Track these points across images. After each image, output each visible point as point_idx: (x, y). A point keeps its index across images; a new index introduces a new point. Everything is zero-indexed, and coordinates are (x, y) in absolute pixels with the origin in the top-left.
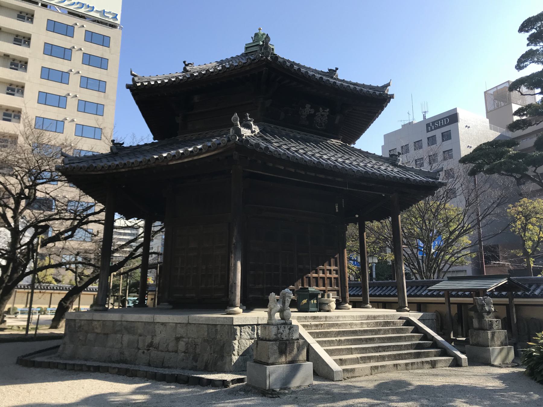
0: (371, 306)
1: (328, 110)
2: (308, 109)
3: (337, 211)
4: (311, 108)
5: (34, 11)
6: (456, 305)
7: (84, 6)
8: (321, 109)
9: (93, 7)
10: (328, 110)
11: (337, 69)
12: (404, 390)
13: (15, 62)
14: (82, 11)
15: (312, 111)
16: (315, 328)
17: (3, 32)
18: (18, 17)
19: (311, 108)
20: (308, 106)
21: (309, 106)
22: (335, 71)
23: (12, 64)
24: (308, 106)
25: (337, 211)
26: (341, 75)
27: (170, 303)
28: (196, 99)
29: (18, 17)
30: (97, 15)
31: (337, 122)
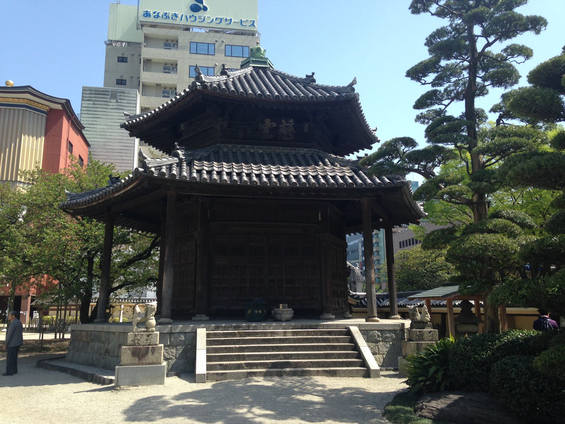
0: (399, 317)
1: (292, 120)
2: (268, 123)
3: (320, 219)
4: (271, 122)
5: (178, 37)
6: (440, 315)
7: (223, 21)
8: (283, 121)
9: (231, 20)
10: (292, 120)
11: (313, 74)
12: (34, 354)
13: (167, 89)
14: (223, 25)
15: (274, 125)
16: (291, 334)
17: (154, 63)
18: (165, 46)
19: (271, 122)
20: (268, 121)
21: (270, 120)
22: (312, 76)
23: (164, 93)
24: (268, 121)
25: (320, 219)
26: (320, 81)
27: (208, 315)
28: (182, 127)
29: (165, 46)
30: (239, 27)
31: (306, 130)
